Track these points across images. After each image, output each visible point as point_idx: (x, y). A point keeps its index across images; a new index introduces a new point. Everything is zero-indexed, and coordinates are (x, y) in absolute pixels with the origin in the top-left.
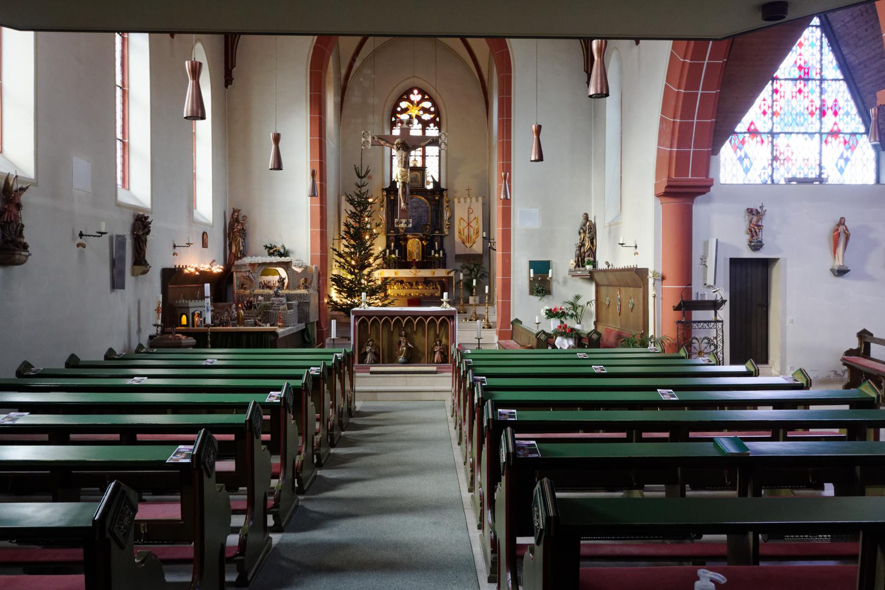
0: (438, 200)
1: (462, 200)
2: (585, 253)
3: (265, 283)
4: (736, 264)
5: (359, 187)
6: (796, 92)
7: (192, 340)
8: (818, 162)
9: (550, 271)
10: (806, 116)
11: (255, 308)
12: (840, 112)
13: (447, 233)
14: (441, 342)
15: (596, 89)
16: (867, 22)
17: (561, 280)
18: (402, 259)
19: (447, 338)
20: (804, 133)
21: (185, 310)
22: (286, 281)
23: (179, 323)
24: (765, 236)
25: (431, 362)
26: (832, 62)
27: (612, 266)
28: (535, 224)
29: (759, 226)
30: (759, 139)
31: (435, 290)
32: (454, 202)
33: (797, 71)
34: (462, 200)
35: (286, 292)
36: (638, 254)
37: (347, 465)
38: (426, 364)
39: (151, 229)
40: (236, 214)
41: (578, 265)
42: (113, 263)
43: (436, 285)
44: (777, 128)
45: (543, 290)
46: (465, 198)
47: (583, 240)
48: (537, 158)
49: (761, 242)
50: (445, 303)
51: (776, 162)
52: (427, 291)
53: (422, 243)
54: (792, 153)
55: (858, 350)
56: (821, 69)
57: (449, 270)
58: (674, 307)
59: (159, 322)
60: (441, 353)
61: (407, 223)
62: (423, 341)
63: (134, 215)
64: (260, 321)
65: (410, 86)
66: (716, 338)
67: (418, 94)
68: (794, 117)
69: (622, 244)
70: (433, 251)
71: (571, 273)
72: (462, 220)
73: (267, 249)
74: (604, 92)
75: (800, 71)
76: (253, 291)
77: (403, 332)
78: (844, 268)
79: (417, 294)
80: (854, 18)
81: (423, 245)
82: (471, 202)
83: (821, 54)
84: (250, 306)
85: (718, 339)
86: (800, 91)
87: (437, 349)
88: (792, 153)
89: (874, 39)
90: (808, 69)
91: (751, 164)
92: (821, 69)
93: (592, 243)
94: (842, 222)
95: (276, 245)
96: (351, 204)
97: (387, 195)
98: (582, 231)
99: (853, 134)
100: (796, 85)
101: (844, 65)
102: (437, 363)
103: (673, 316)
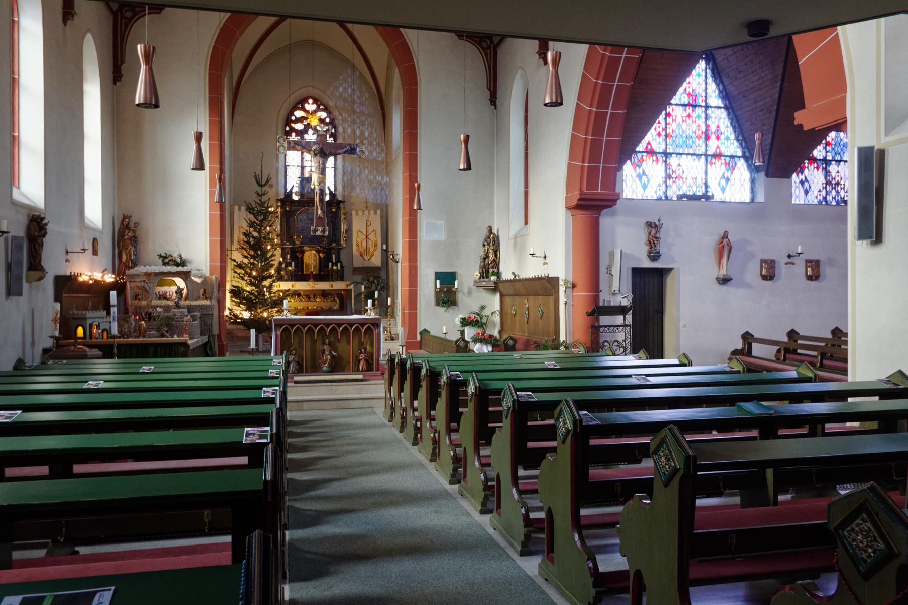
0: (335, 213)
1: (360, 213)
2: (489, 264)
3: (160, 295)
4: (637, 272)
5: (260, 195)
6: (686, 117)
7: (96, 352)
8: (704, 181)
9: (456, 282)
10: (694, 139)
11: (154, 319)
12: (722, 137)
13: (344, 246)
14: (365, 350)
15: (552, 99)
16: (747, 57)
17: (466, 291)
18: (298, 272)
19: (372, 345)
20: (692, 155)
21: (81, 321)
22: (184, 292)
23: (73, 334)
24: (662, 248)
25: (356, 370)
26: (715, 91)
27: (518, 276)
28: (440, 236)
29: (657, 238)
30: (655, 158)
31: (333, 303)
32: (351, 215)
33: (686, 98)
34: (360, 213)
35: (187, 303)
36: (547, 264)
37: (312, 467)
38: (351, 373)
39: (48, 231)
40: (127, 220)
41: (482, 277)
42: (9, 268)
43: (334, 298)
44: (670, 149)
45: (449, 301)
46: (363, 211)
47: (487, 252)
48: (465, 167)
49: (659, 253)
50: (369, 310)
51: (670, 180)
52: (325, 304)
53: (319, 255)
54: (683, 172)
55: (742, 350)
56: (706, 97)
57: (348, 283)
58: (587, 312)
59: (57, 334)
60: (366, 361)
61: (324, 231)
62: (348, 349)
63: (29, 215)
64: (167, 332)
65: (305, 95)
66: (625, 341)
67: (312, 104)
68: (684, 139)
69: (532, 254)
70: (330, 264)
71: (475, 284)
72: (359, 233)
73: (161, 259)
74: (559, 101)
75: (689, 98)
76: (151, 302)
77: (327, 340)
78: (727, 277)
79: (315, 307)
80: (736, 53)
81: (320, 257)
82: (369, 214)
83: (706, 83)
84: (150, 317)
85: (627, 342)
86: (689, 116)
87: (362, 356)
88: (683, 172)
89: (752, 72)
90: (696, 96)
91: (649, 181)
92: (706, 97)
93: (496, 255)
94: (726, 236)
95: (172, 254)
96: (250, 213)
97: (282, 206)
98: (486, 243)
99: (732, 157)
100: (685, 110)
101: (725, 95)
102: (362, 371)
103: (582, 320)
